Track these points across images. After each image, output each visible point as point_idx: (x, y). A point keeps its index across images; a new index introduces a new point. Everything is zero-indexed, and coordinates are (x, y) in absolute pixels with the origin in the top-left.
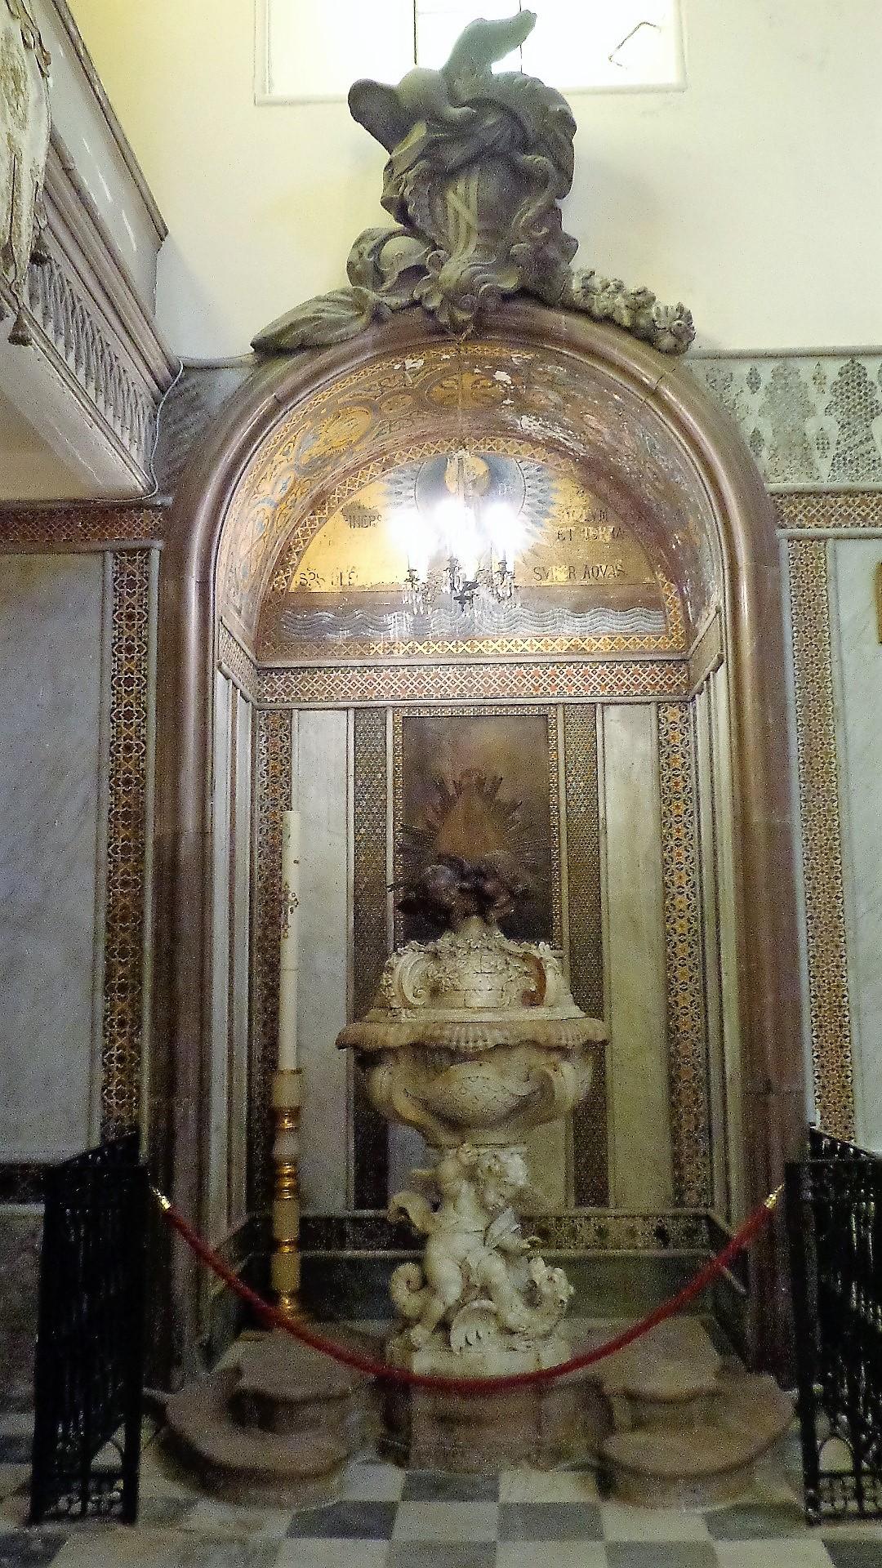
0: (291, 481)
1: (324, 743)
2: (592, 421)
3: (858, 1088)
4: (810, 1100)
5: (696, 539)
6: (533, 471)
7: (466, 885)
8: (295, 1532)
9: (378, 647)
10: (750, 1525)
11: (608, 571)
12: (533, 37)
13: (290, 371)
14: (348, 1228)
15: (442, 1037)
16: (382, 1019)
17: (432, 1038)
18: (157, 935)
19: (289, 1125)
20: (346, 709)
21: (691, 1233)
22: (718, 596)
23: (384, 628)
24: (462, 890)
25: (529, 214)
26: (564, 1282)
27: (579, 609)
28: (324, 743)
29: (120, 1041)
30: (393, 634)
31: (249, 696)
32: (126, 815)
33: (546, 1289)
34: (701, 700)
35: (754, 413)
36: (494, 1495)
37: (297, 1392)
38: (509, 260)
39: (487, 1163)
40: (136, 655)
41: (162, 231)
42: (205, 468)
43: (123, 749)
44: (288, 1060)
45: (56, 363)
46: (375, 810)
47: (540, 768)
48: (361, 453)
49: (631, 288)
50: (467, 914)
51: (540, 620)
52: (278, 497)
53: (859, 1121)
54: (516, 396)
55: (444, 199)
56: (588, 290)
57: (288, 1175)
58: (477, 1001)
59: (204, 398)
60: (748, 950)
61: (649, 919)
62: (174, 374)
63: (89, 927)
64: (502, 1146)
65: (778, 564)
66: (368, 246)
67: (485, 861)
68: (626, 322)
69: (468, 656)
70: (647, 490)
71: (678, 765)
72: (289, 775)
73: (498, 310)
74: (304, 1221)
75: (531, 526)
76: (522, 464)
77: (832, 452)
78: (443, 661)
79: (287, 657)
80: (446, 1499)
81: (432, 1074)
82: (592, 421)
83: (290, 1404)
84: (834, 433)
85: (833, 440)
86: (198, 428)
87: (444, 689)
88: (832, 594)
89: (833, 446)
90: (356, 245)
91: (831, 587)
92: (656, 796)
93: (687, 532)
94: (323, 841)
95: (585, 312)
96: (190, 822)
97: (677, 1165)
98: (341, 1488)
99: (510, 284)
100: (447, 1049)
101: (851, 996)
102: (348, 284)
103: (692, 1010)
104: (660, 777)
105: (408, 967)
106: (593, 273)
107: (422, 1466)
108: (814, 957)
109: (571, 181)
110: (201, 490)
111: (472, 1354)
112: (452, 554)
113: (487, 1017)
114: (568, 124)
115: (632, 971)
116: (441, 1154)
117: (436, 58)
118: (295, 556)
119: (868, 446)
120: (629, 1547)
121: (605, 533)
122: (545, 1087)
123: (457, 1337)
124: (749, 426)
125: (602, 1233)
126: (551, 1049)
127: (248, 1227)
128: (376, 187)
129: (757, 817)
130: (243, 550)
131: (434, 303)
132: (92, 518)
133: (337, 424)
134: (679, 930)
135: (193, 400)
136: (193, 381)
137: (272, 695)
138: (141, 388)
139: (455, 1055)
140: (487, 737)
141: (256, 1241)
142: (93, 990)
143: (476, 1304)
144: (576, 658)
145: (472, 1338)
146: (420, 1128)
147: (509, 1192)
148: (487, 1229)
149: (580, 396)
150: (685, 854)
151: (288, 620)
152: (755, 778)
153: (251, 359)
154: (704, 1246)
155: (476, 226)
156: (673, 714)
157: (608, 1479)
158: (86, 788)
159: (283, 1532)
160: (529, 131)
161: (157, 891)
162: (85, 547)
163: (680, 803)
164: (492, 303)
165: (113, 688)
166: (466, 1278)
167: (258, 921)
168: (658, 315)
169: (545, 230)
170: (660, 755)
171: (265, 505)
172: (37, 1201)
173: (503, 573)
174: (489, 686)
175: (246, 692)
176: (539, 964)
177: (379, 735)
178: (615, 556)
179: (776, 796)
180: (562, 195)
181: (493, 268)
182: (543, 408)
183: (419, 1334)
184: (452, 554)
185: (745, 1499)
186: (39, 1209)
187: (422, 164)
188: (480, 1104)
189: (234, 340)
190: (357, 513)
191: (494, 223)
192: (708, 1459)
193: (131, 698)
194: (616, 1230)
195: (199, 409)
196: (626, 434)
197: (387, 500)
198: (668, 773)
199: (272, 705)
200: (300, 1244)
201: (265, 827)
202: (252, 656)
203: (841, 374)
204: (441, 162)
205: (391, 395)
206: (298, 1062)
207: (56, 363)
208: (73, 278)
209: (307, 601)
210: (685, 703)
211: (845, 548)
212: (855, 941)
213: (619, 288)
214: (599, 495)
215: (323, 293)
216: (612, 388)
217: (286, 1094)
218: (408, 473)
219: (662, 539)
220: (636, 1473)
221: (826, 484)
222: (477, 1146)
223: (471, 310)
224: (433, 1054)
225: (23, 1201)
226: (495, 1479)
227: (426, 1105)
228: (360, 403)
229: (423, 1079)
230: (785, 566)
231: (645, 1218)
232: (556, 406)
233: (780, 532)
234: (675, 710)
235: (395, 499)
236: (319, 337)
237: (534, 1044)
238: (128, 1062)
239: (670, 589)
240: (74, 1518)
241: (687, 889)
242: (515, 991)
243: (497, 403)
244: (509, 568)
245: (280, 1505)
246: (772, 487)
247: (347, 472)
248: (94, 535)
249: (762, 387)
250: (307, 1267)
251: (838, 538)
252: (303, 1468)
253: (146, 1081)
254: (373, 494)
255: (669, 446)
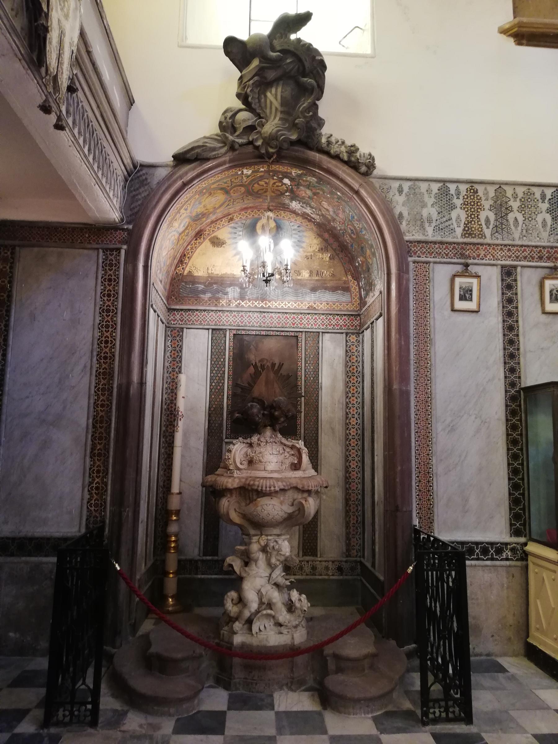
0: (187, 223)
1: (197, 346)
2: (325, 204)
3: (435, 510)
4: (414, 514)
5: (370, 261)
6: (296, 227)
7: (266, 412)
8: (178, 730)
9: (223, 302)
10: (396, 725)
11: (327, 273)
12: (309, 24)
13: (190, 170)
14: (200, 564)
15: (254, 485)
16: (225, 474)
17: (249, 485)
18: (117, 430)
19: (175, 518)
20: (208, 329)
21: (353, 569)
22: (380, 285)
23: (226, 294)
24: (263, 414)
25: (304, 105)
26: (306, 601)
27: (314, 290)
28: (197, 346)
29: (97, 480)
30: (230, 296)
31: (164, 321)
32: (104, 374)
33: (298, 605)
34: (367, 333)
35: (400, 204)
36: (271, 706)
37: (179, 656)
38: (294, 126)
39: (272, 545)
40: (112, 299)
41: (132, 101)
42: (148, 212)
43: (104, 342)
44: (175, 489)
45: (79, 149)
46: (219, 375)
47: (294, 360)
48: (219, 214)
49: (349, 143)
50: (265, 426)
51: (296, 294)
52: (181, 229)
53: (436, 525)
54: (292, 191)
55: (266, 96)
56: (329, 143)
57: (174, 541)
58: (270, 467)
59: (149, 181)
60: (389, 445)
61: (339, 428)
62: (135, 167)
63: (84, 425)
64: (278, 535)
65: (408, 274)
66: (229, 114)
67: (275, 401)
68: (346, 158)
69: (264, 308)
70: (347, 238)
71: (354, 361)
72: (181, 357)
73: (287, 149)
74: (179, 561)
75: (297, 248)
76: (291, 224)
77: (434, 224)
78: (253, 310)
79: (182, 304)
80: (249, 709)
81: (248, 501)
82: (325, 204)
83: (176, 661)
84: (435, 216)
85: (434, 219)
86: (145, 194)
87: (253, 322)
88: (431, 288)
89: (434, 221)
90: (224, 114)
91: (431, 284)
92: (344, 376)
93: (365, 258)
94: (195, 389)
95: (327, 153)
96: (135, 378)
97: (348, 538)
98: (198, 704)
99: (294, 137)
100: (257, 490)
101: (434, 468)
102: (218, 131)
103: (356, 470)
104: (346, 366)
105: (238, 450)
106: (331, 135)
107: (237, 689)
108: (417, 450)
109: (323, 93)
110: (144, 227)
111: (262, 636)
112: (256, 265)
113: (275, 475)
114: (322, 66)
115: (331, 449)
116: (250, 539)
117: (264, 28)
118: (187, 259)
119: (449, 223)
120: (341, 737)
121: (326, 256)
122: (301, 509)
123: (255, 628)
124: (397, 212)
125: (314, 568)
126: (303, 491)
127: (154, 565)
128: (234, 88)
129: (395, 386)
130: (164, 254)
131: (259, 143)
132: (92, 233)
133: (210, 198)
134: (352, 434)
135: (143, 180)
136: (144, 172)
137: (174, 321)
138: (119, 172)
139: (261, 493)
140: (271, 345)
141: (158, 571)
142: (85, 456)
143: (265, 612)
144: (312, 311)
145: (262, 628)
146: (240, 526)
147: (282, 558)
148: (270, 575)
149: (321, 193)
150: (356, 400)
151: (183, 289)
152: (395, 368)
153: (172, 163)
154: (358, 575)
155: (279, 108)
156: (353, 338)
157: (328, 699)
158: (85, 360)
159: (171, 730)
160: (306, 67)
161: (118, 409)
162: (89, 246)
163: (355, 377)
164: (285, 145)
165: (101, 298)
166: (261, 599)
167: (164, 423)
168: (360, 156)
169: (311, 113)
170: (347, 356)
171: (175, 233)
172: (53, 556)
173: (286, 269)
174: (273, 322)
175: (163, 319)
176: (299, 451)
177: (223, 342)
178: (330, 267)
179: (404, 378)
180: (319, 99)
181: (286, 129)
182: (303, 198)
183: (237, 626)
184: (256, 265)
185: (390, 708)
186: (54, 559)
187: (256, 78)
188: (271, 517)
189: (165, 156)
190: (216, 240)
191: (288, 108)
192: (374, 691)
193: (109, 318)
194: (320, 567)
195: (146, 185)
196: (340, 212)
197: (230, 236)
198: (350, 364)
199: (174, 326)
200: (176, 573)
201: (169, 380)
202: (166, 303)
203: (439, 190)
204: (266, 78)
205: (235, 187)
206: (180, 489)
207: (79, 149)
208: (87, 108)
209: (192, 279)
210: (359, 333)
211: (438, 267)
212: (436, 444)
213: (343, 143)
214: (326, 240)
215: (208, 135)
216: (337, 189)
217: (174, 503)
218: (240, 224)
219: (352, 260)
220: (342, 697)
221: (430, 238)
222: (267, 535)
223: (276, 147)
224: (250, 493)
225: (46, 556)
226: (271, 696)
227: (244, 516)
228: (222, 189)
229: (243, 504)
230: (411, 275)
231: (333, 562)
232: (309, 197)
233: (410, 259)
234: (354, 336)
235: (234, 236)
236: (206, 155)
237: (296, 488)
238: (100, 490)
239: (354, 283)
240: (65, 725)
241: (356, 416)
242: (288, 462)
243: (282, 194)
244: (289, 267)
245: (170, 715)
246: (406, 238)
247: (212, 222)
248: (94, 241)
249: (404, 193)
250: (180, 583)
251: (435, 263)
252: (181, 696)
253: (109, 499)
254: (223, 233)
255: (361, 218)
